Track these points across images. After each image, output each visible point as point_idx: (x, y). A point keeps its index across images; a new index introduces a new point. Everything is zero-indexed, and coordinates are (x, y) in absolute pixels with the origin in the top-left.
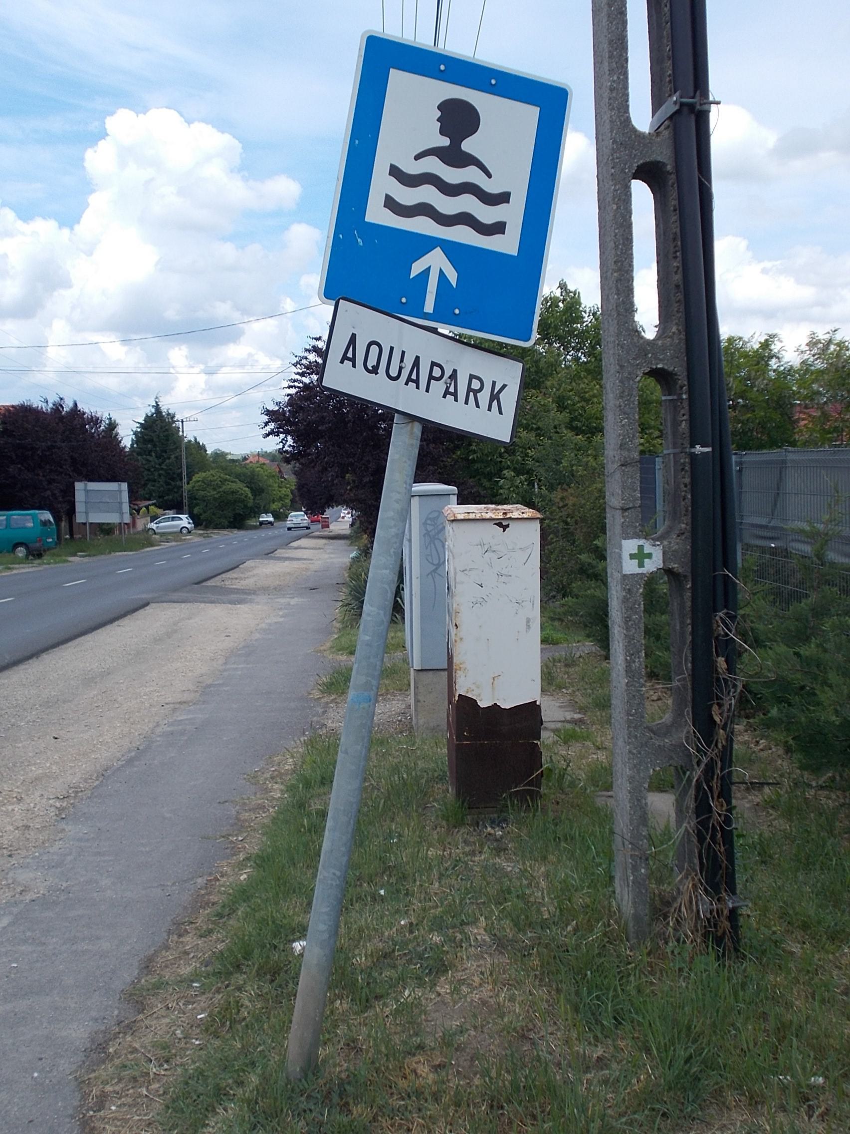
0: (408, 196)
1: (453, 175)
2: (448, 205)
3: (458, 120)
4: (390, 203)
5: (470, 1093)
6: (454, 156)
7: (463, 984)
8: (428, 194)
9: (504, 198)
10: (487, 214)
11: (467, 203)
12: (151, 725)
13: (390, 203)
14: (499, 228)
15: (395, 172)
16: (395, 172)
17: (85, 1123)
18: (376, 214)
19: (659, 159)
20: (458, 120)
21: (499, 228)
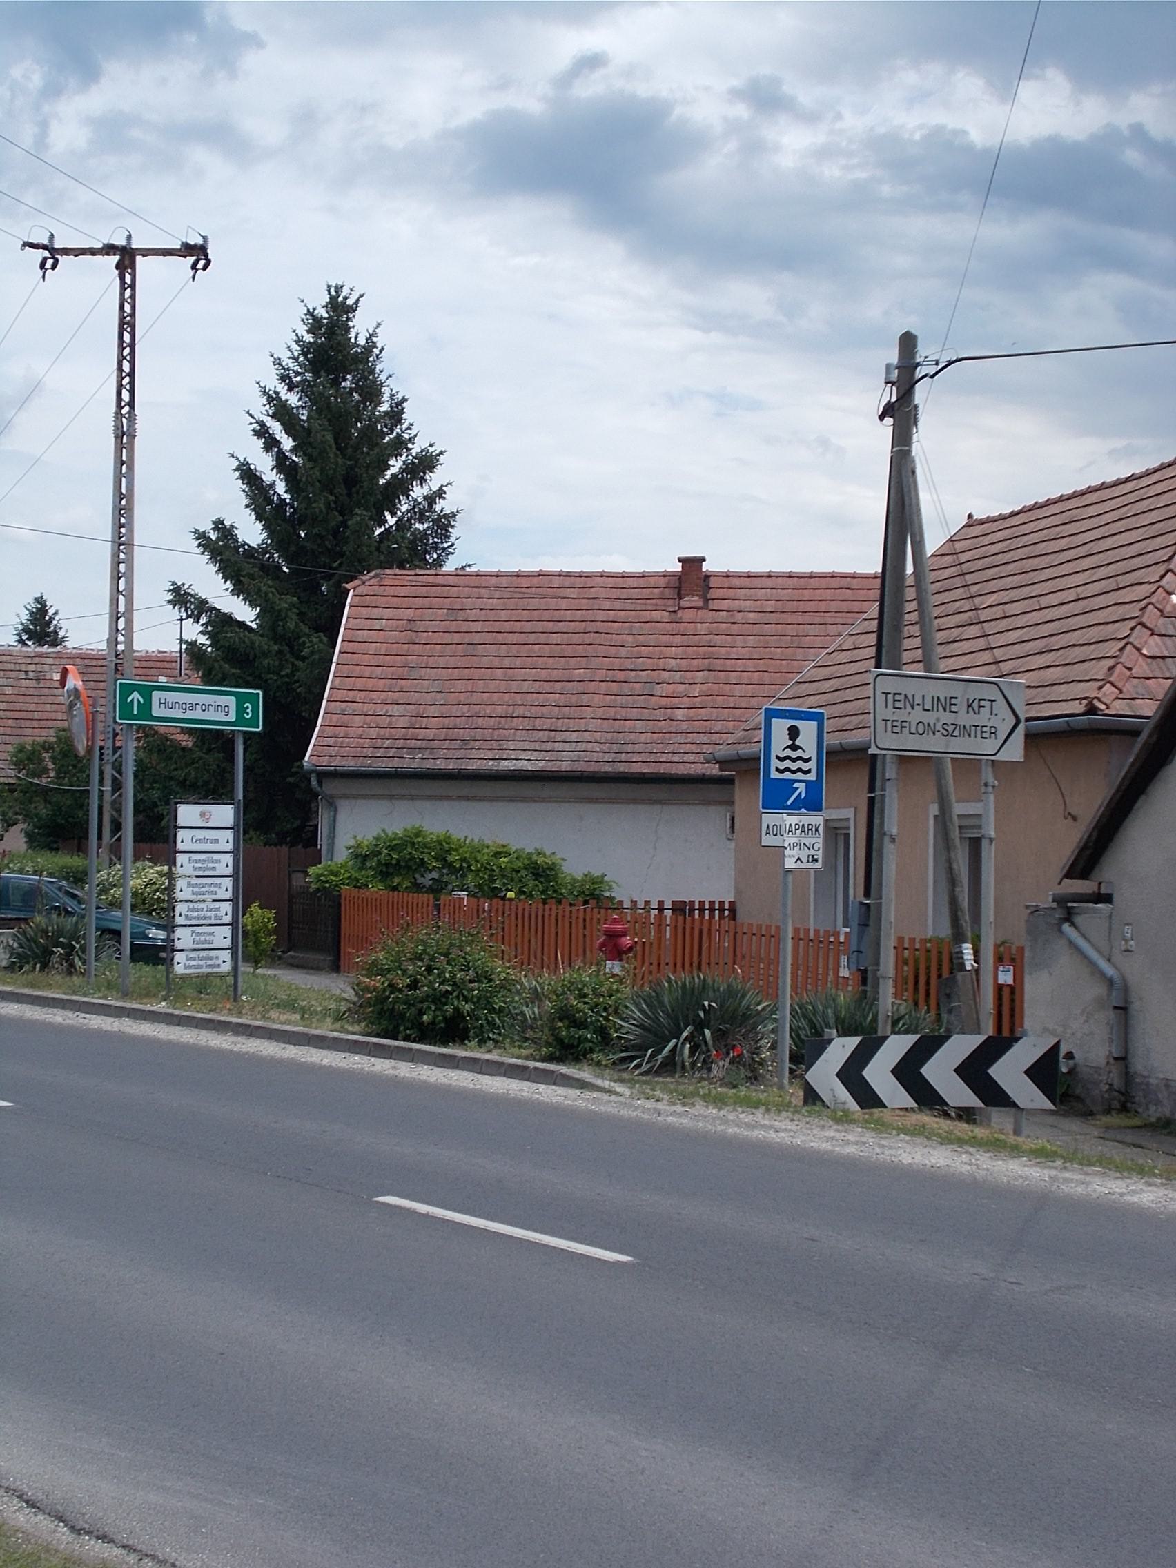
0: (782, 765)
1: (794, 754)
2: (794, 766)
3: (794, 732)
4: (777, 770)
5: (491, 928)
6: (794, 747)
7: (696, 1029)
8: (788, 763)
9: (809, 759)
10: (805, 767)
11: (799, 764)
12: (87, 1526)
13: (777, 770)
14: (809, 771)
15: (778, 757)
16: (778, 757)
17: (1165, 1126)
18: (774, 775)
19: (658, 85)
20: (794, 732)
21: (809, 771)
